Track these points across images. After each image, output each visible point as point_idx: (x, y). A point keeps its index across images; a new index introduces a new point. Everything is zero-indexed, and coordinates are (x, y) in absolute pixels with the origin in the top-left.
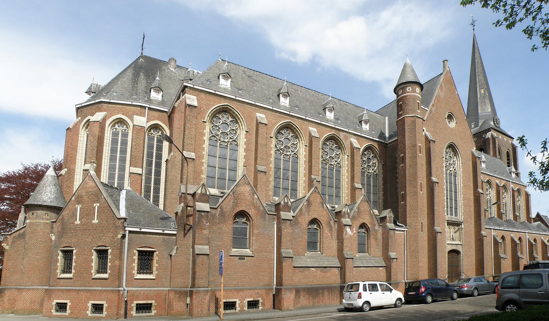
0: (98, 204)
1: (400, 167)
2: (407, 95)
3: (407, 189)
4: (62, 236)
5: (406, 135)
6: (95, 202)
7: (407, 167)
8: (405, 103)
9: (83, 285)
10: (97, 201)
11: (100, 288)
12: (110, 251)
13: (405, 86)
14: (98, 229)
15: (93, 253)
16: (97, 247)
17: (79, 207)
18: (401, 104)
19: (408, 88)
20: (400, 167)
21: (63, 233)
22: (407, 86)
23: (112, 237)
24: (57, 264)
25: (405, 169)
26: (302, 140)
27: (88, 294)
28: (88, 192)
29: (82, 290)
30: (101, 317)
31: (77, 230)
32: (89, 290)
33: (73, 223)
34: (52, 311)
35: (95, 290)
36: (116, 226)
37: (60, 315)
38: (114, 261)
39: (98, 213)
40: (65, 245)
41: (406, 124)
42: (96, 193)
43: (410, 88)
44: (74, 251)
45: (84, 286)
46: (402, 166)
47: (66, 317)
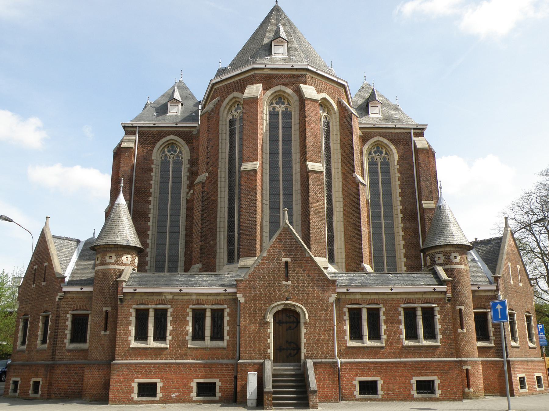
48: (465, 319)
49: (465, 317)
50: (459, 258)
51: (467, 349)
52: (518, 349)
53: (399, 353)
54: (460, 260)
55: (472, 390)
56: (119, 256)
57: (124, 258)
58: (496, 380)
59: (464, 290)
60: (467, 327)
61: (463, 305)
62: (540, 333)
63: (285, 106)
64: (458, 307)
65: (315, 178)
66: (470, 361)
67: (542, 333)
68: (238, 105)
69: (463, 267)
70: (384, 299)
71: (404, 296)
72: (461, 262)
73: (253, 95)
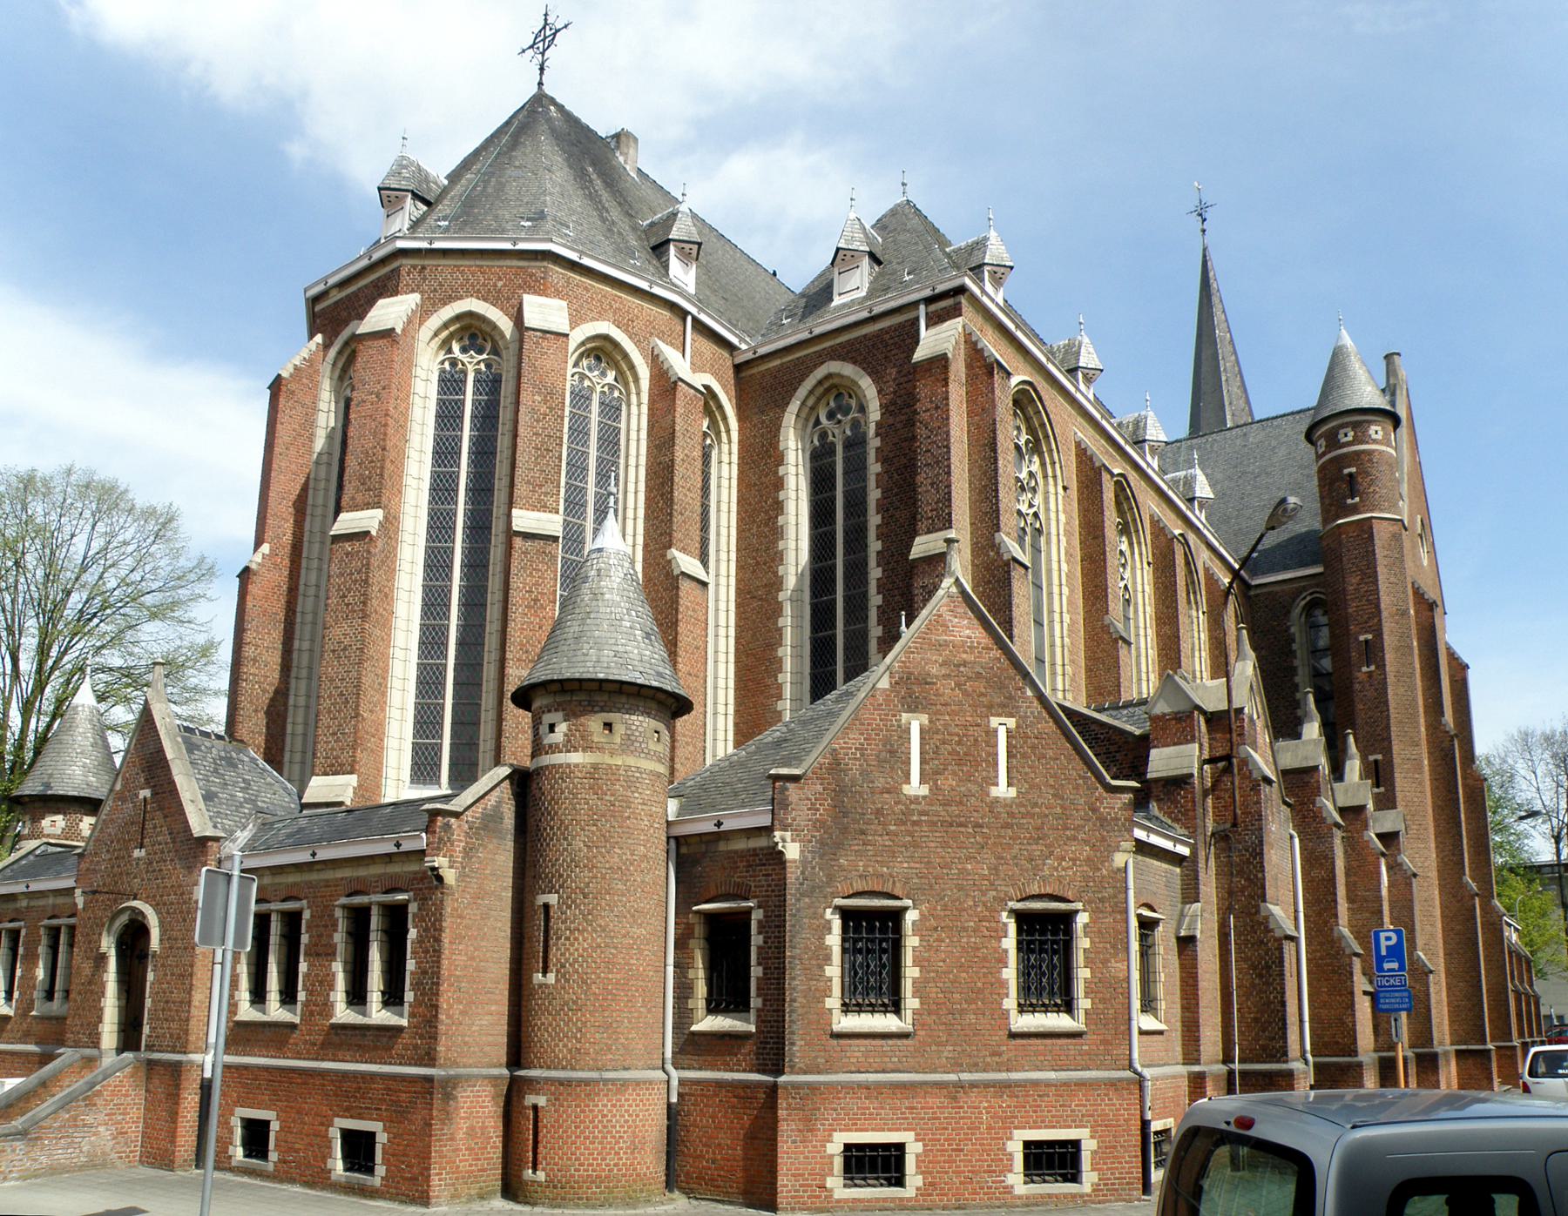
0: (1012, 723)
1: (1359, 674)
2: (1374, 451)
3: (1395, 749)
4: (839, 845)
5: (1380, 577)
6: (992, 710)
7: (1391, 679)
8: (1368, 474)
9: (966, 1061)
10: (1003, 706)
11: (1052, 1075)
12: (1082, 919)
13: (1364, 421)
14: (1020, 826)
15: (1005, 925)
16: (849, 897)
17: (915, 724)
18: (1350, 475)
19: (1373, 428)
20: (1359, 674)
21: (844, 830)
22: (1370, 422)
23: (1088, 859)
24: (821, 968)
25: (1384, 683)
26: (1139, 543)
27: (1006, 1102)
28: (959, 666)
29: (973, 1085)
30: (1074, 1196)
31: (915, 823)
32: (1007, 1085)
33: (894, 790)
34: (828, 1186)
35: (1035, 1083)
36: (1103, 820)
37: (869, 1201)
38: (1105, 962)
39: (1010, 755)
40: (859, 886)
41: (1377, 541)
42: (995, 675)
43: (1379, 428)
44: (911, 917)
45: (974, 1067)
46: (1370, 674)
47: (902, 1205)
48: (559, 938)
49: (555, 934)
50: (562, 728)
51: (553, 1040)
52: (905, 1042)
53: (324, 1045)
54: (566, 735)
55: (541, 1176)
56: (35, 820)
57: (46, 823)
58: (739, 1151)
59: (566, 839)
60: (563, 966)
61: (557, 892)
62: (1387, 966)
63: (485, 356)
64: (542, 899)
65: (347, 554)
66: (547, 1080)
67: (1395, 965)
68: (839, 395)
69: (576, 758)
70: (309, 884)
71: (347, 873)
72: (569, 741)
73: (938, 350)
